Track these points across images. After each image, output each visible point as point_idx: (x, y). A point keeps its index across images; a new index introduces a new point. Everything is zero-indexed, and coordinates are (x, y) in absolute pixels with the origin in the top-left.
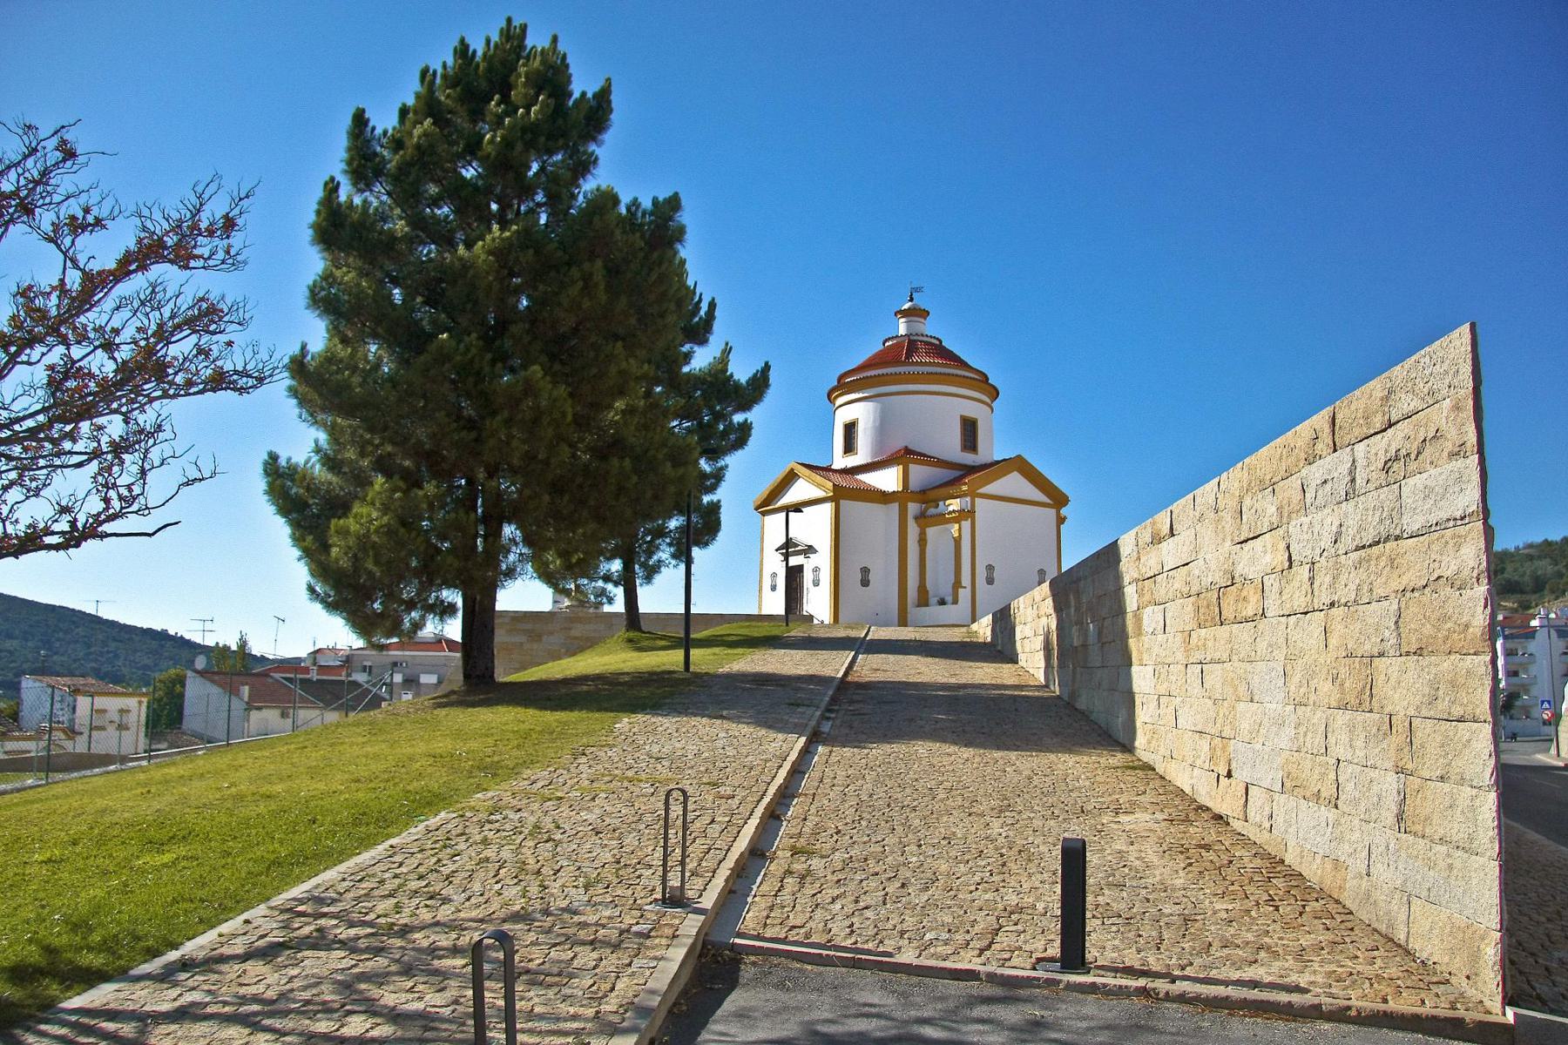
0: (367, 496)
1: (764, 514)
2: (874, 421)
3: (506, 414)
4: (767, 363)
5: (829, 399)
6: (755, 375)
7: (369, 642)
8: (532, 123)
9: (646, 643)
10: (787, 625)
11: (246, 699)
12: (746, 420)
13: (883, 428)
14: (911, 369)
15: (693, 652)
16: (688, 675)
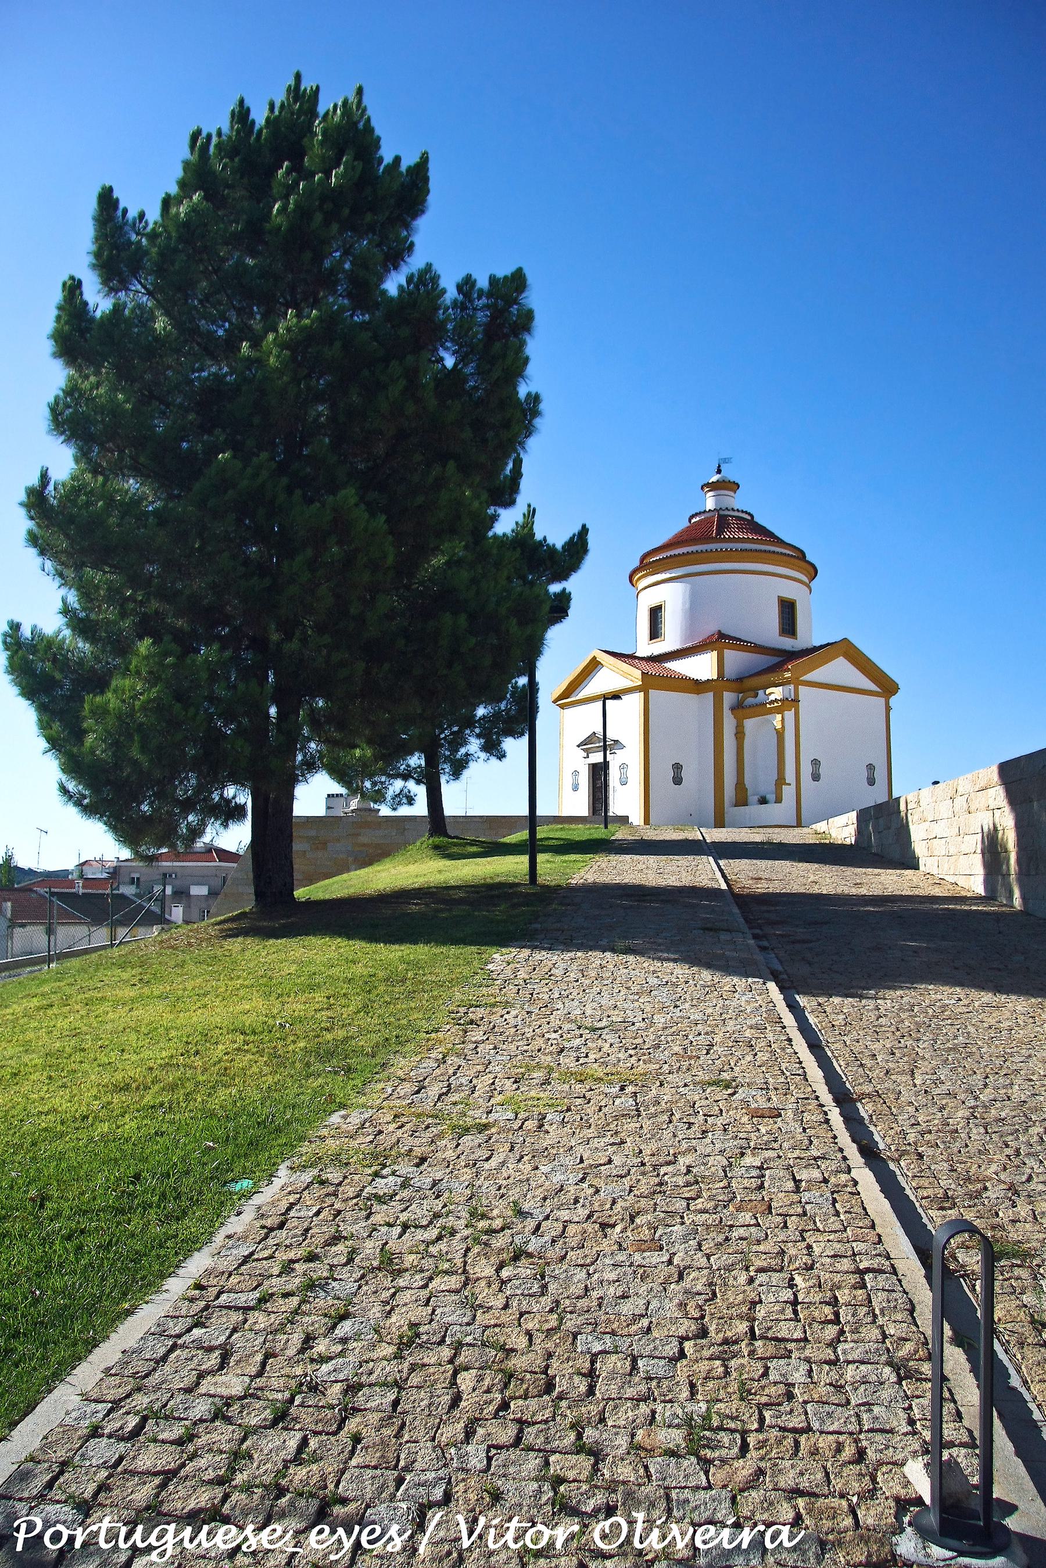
0: (130, 663)
1: (562, 707)
2: (684, 604)
3: (309, 552)
4: (584, 526)
5: (631, 581)
6: (572, 539)
7: (136, 853)
8: (333, 190)
9: (455, 850)
10: (606, 827)
11: (9, 915)
12: (564, 589)
13: (694, 610)
14: (724, 546)
15: (541, 858)
16: (531, 890)
